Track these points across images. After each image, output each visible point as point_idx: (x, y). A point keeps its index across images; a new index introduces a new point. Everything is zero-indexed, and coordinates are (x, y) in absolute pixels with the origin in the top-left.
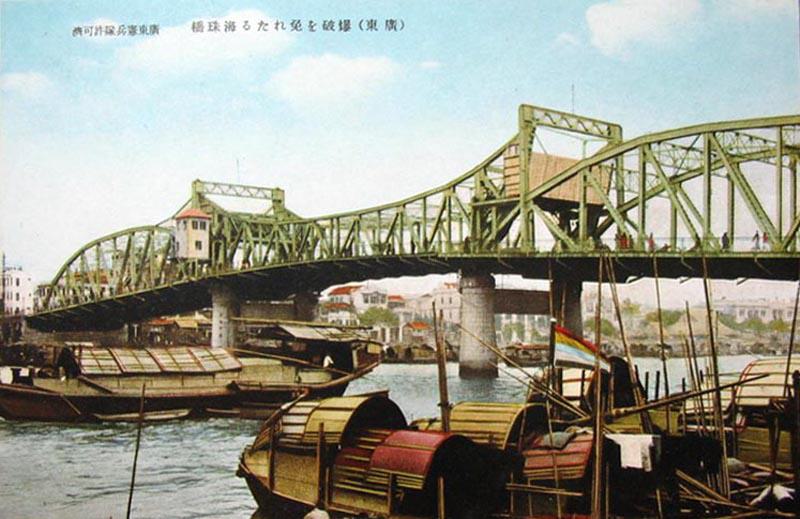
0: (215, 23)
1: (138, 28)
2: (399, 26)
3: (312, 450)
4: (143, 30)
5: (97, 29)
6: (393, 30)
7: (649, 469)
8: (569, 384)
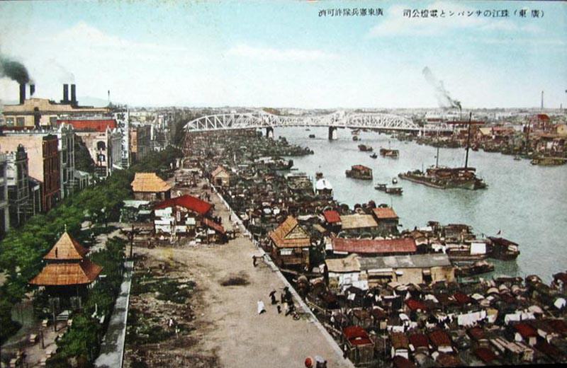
0: (506, 11)
1: (367, 10)
2: (540, 15)
3: (20, 217)
4: (371, 12)
5: (337, 12)
6: (380, 15)
7: (83, 229)
8: (436, 152)
